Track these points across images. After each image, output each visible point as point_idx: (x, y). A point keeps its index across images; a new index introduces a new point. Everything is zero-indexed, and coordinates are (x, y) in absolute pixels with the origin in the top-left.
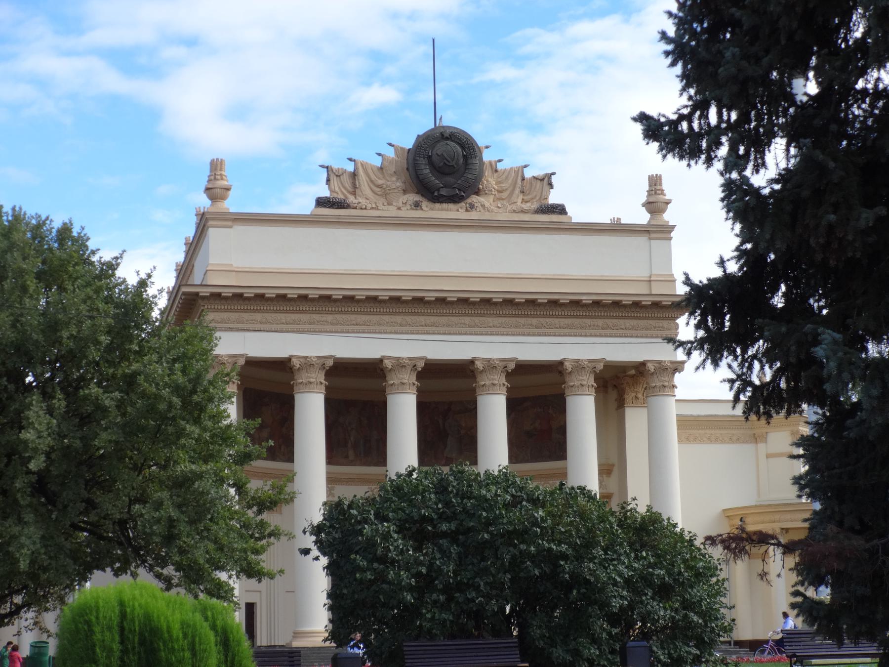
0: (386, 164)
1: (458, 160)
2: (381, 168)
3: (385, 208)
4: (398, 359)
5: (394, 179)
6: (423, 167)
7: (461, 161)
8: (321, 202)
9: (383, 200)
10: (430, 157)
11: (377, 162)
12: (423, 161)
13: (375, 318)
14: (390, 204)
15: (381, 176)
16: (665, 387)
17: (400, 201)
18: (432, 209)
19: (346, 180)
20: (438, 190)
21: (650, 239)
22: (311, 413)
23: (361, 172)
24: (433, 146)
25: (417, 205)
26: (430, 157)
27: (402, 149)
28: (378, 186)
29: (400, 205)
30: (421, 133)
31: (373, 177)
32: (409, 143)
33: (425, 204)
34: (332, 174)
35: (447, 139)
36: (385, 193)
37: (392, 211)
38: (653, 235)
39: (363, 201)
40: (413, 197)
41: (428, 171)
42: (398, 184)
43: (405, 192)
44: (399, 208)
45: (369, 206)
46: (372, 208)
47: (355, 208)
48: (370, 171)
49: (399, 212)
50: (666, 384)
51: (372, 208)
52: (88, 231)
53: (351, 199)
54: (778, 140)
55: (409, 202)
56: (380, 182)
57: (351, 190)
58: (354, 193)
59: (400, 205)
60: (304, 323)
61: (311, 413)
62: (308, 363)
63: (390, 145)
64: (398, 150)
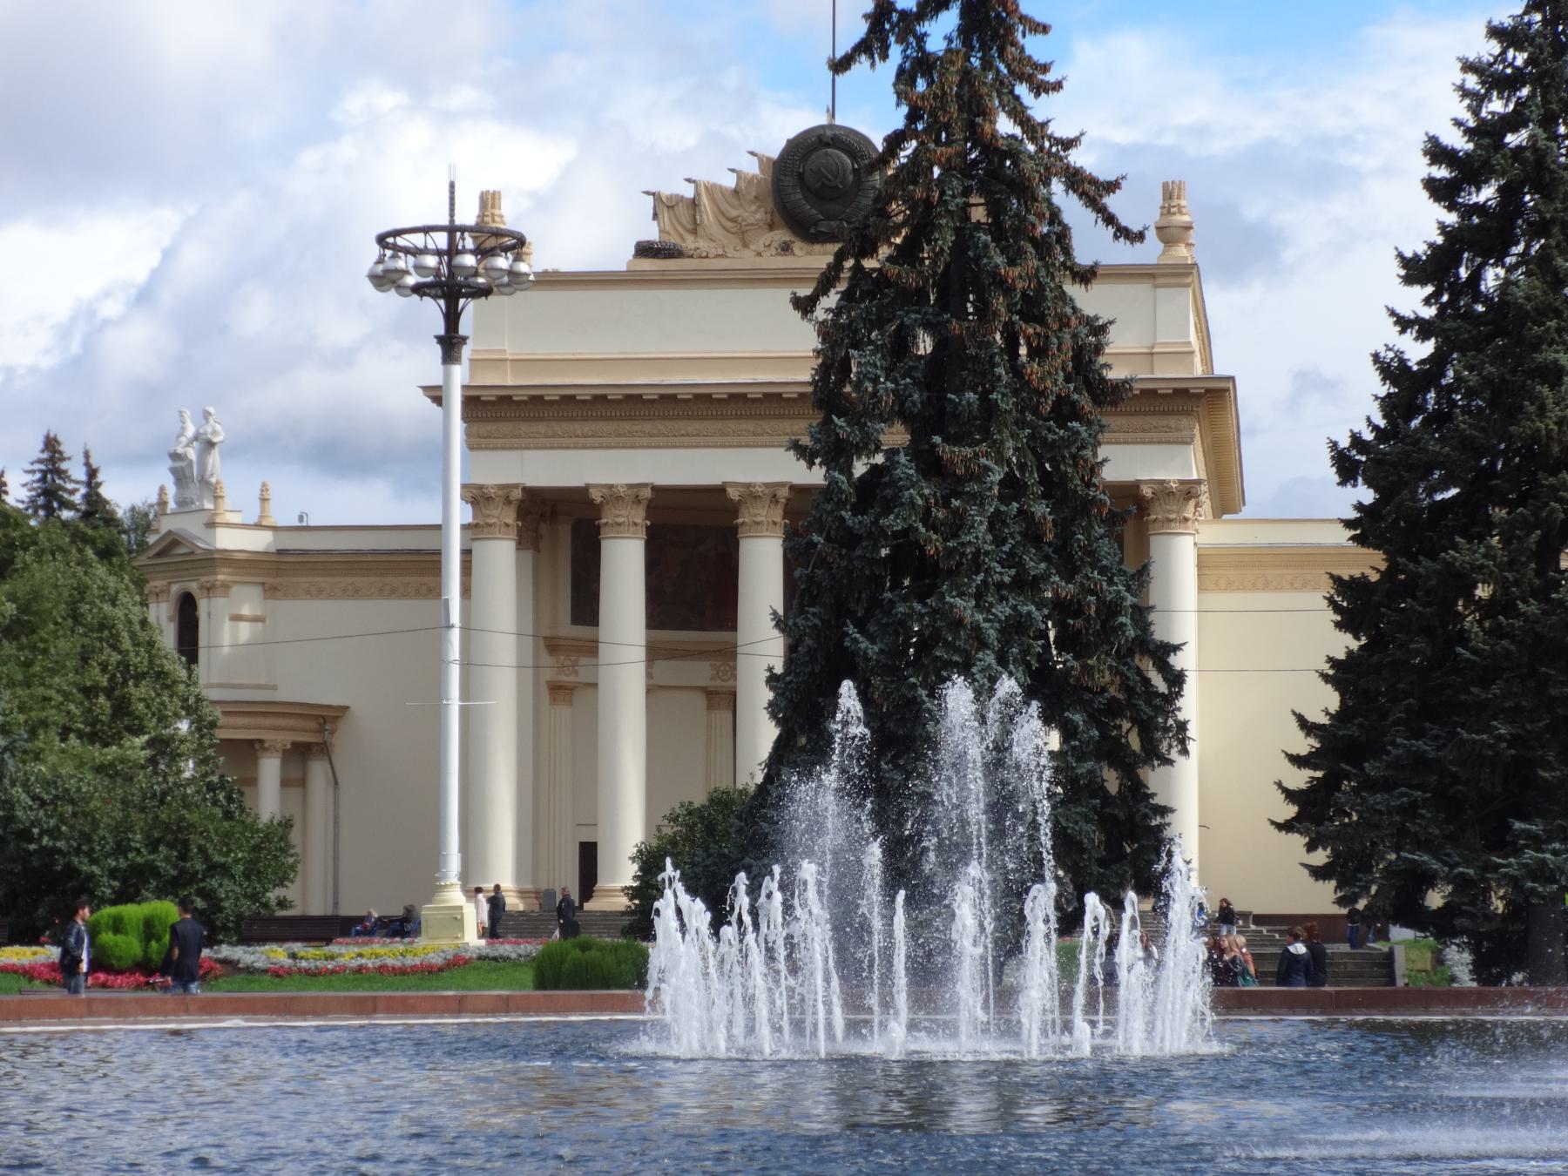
0: (743, 186)
1: (845, 177)
2: (736, 192)
3: (737, 254)
4: (749, 485)
5: (753, 208)
6: (790, 190)
7: (851, 178)
8: (645, 250)
9: (735, 240)
10: (801, 176)
11: (730, 182)
12: (790, 181)
13: (610, 426)
14: (745, 245)
15: (736, 202)
16: (1170, 521)
17: (762, 241)
18: (809, 253)
19: (683, 212)
20: (816, 224)
21: (1156, 287)
22: (625, 565)
23: (705, 200)
24: (805, 157)
25: (786, 248)
26: (801, 176)
27: (768, 159)
28: (731, 220)
29: (761, 248)
30: (791, 136)
31: (725, 207)
32: (774, 150)
33: (798, 247)
34: (663, 205)
35: (827, 145)
36: (742, 234)
37: (746, 260)
38: (1160, 281)
39: (703, 245)
40: (781, 235)
41: (799, 196)
42: (758, 216)
43: (771, 227)
44: (759, 254)
45: (713, 252)
46: (718, 256)
47: (691, 257)
48: (718, 196)
49: (759, 259)
50: (1173, 516)
51: (718, 256)
52: (225, 484)
53: (689, 243)
54: (24, 494)
55: (775, 244)
56: (733, 213)
57: (690, 227)
58: (694, 232)
59: (761, 248)
60: (714, 435)
61: (625, 565)
62: (613, 495)
63: (752, 153)
64: (763, 161)
